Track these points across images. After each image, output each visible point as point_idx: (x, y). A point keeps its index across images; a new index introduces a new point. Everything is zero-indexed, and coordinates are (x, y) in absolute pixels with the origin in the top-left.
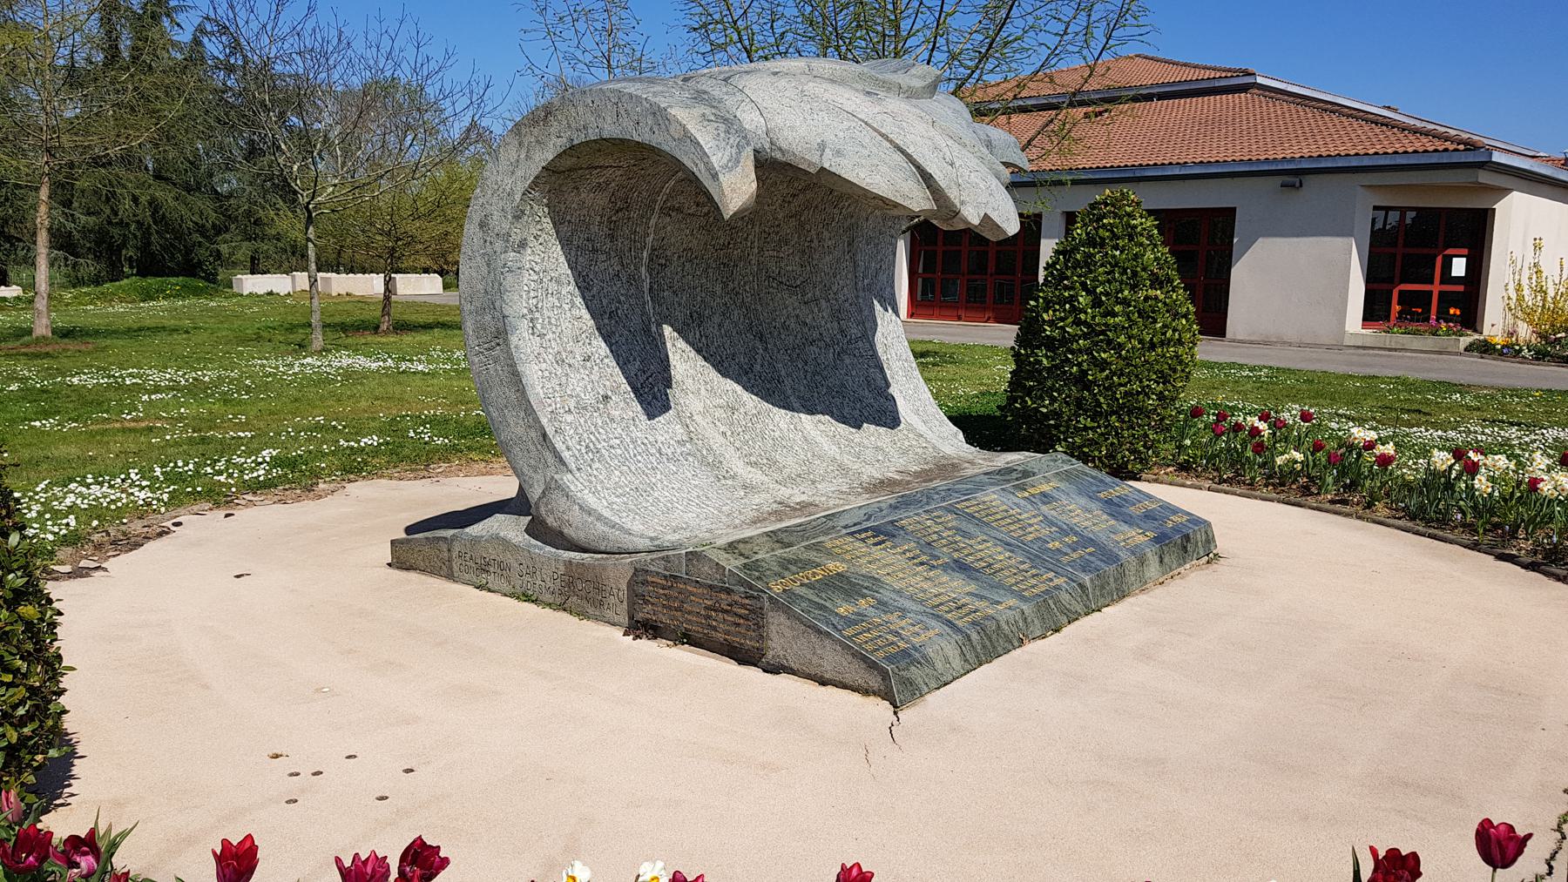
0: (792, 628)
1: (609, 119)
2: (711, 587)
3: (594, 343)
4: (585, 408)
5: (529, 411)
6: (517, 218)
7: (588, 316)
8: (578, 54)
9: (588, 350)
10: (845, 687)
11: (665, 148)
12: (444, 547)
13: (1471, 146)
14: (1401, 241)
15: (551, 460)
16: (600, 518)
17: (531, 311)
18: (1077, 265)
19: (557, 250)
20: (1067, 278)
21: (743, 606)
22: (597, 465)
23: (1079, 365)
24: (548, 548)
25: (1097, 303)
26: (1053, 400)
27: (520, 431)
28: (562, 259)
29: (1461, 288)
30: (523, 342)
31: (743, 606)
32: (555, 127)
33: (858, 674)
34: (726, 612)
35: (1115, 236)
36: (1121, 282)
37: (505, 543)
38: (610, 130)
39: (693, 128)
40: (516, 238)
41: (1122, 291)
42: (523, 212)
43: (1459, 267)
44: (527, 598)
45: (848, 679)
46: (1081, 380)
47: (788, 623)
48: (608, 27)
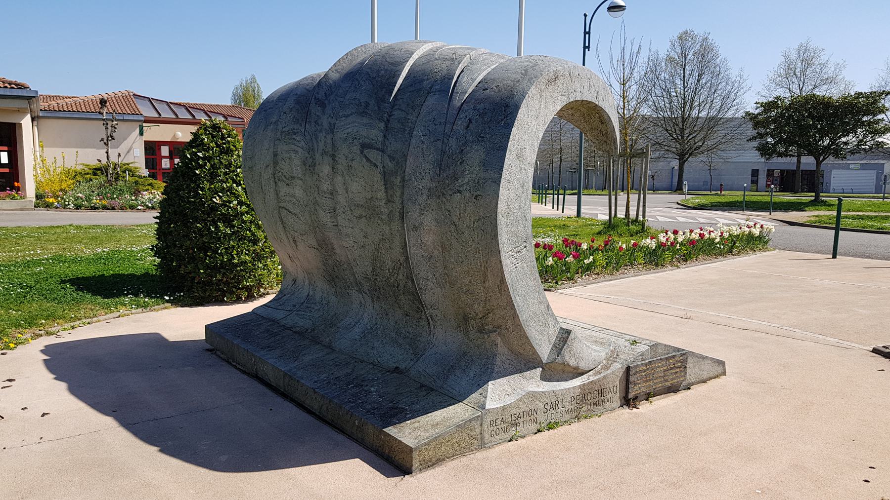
13: (21, 87)
29: (7, 170)
37: (533, 395)
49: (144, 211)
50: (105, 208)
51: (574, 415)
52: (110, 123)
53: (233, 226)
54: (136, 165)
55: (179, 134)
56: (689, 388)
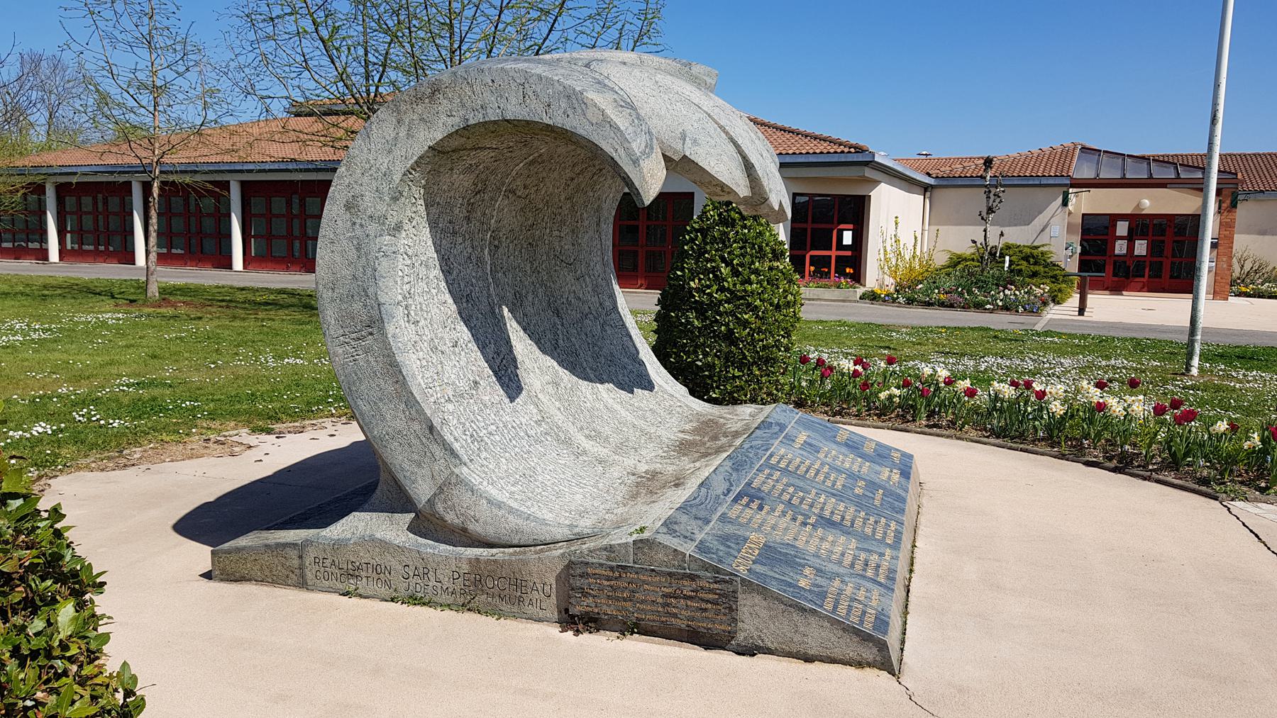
0: (770, 609)
1: (513, 101)
2: (670, 574)
3: (458, 327)
4: (462, 396)
5: (410, 401)
6: (395, 199)
7: (450, 301)
8: (116, 33)
9: (454, 335)
10: (833, 661)
11: (581, 132)
12: (294, 554)
13: (860, 150)
14: (810, 218)
15: (438, 451)
16: (511, 510)
17: (405, 298)
18: (714, 240)
19: (426, 233)
20: (706, 252)
21: (711, 591)
22: (484, 455)
23: (727, 325)
24: (443, 547)
25: (735, 273)
26: (706, 355)
27: (400, 424)
28: (430, 243)
29: (849, 253)
30: (400, 331)
31: (711, 591)
32: (445, 105)
33: (852, 649)
34: (690, 598)
35: (743, 218)
36: (752, 256)
37: (385, 546)
38: (514, 110)
39: (611, 112)
40: (392, 221)
41: (753, 263)
42: (401, 193)
43: (848, 238)
44: (414, 600)
45: (836, 653)
46: (730, 338)
48: (147, 10)
49: (991, 311)
50: (942, 305)
51: (461, 600)
52: (993, 190)
53: (707, 318)
54: (1052, 249)
55: (1147, 202)
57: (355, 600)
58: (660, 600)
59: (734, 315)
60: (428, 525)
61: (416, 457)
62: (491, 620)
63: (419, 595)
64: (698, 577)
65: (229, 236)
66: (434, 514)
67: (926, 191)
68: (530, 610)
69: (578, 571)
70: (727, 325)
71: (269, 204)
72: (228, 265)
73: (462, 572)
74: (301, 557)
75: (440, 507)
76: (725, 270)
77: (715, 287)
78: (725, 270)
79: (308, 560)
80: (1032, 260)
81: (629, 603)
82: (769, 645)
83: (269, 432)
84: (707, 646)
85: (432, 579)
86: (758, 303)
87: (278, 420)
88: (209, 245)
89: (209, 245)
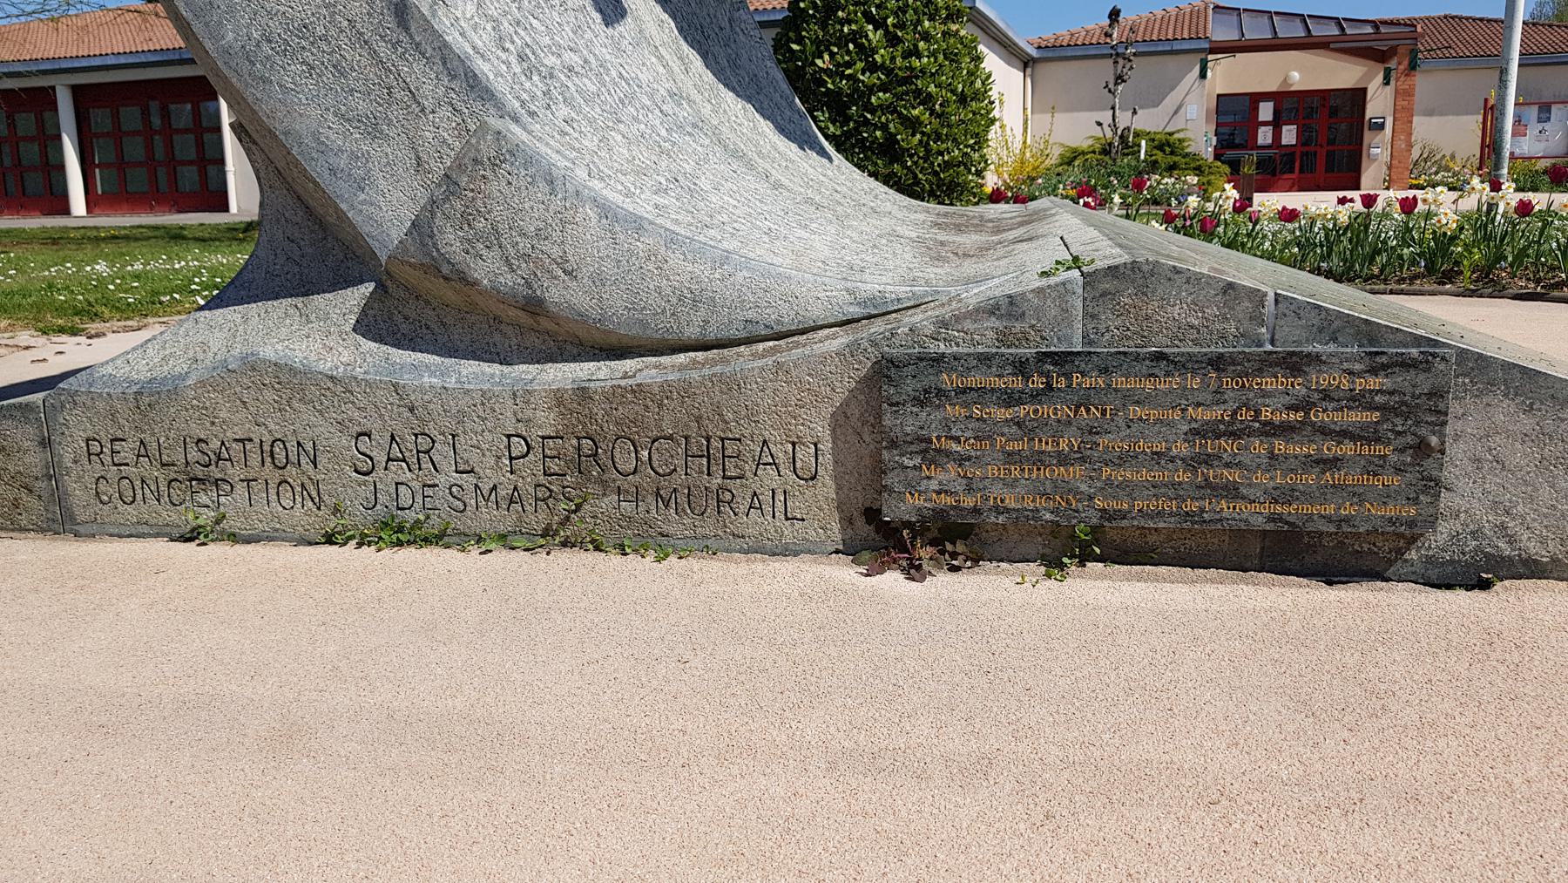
2: (1218, 363)
23: (884, 127)
24: (470, 367)
25: (893, 40)
34: (1285, 430)
36: (916, 11)
37: (290, 382)
44: (397, 532)
47: (1527, 423)
51: (538, 519)
53: (848, 119)
54: (1189, 135)
55: (1296, 75)
56: (1485, 585)
57: (217, 551)
58: (1181, 449)
59: (895, 111)
60: (421, 304)
61: (362, 106)
62: (641, 566)
63: (410, 516)
64: (1315, 359)
65: (61, 168)
66: (434, 267)
67: (1026, 65)
68: (754, 524)
69: (910, 387)
70: (884, 127)
71: (116, 117)
72: (65, 210)
73: (535, 434)
74: (46, 443)
75: (451, 241)
76: (875, 36)
77: (860, 65)
78: (875, 36)
79: (69, 449)
80: (1168, 149)
81: (1077, 471)
82: (1533, 548)
83: (74, 332)
84: (1332, 575)
85: (447, 466)
86: (932, 88)
87: (96, 316)
88: (34, 181)
89: (34, 181)
